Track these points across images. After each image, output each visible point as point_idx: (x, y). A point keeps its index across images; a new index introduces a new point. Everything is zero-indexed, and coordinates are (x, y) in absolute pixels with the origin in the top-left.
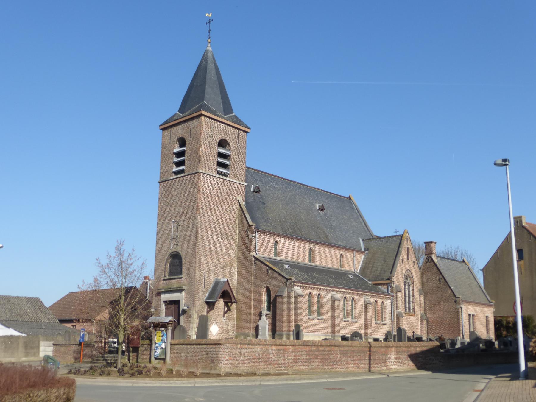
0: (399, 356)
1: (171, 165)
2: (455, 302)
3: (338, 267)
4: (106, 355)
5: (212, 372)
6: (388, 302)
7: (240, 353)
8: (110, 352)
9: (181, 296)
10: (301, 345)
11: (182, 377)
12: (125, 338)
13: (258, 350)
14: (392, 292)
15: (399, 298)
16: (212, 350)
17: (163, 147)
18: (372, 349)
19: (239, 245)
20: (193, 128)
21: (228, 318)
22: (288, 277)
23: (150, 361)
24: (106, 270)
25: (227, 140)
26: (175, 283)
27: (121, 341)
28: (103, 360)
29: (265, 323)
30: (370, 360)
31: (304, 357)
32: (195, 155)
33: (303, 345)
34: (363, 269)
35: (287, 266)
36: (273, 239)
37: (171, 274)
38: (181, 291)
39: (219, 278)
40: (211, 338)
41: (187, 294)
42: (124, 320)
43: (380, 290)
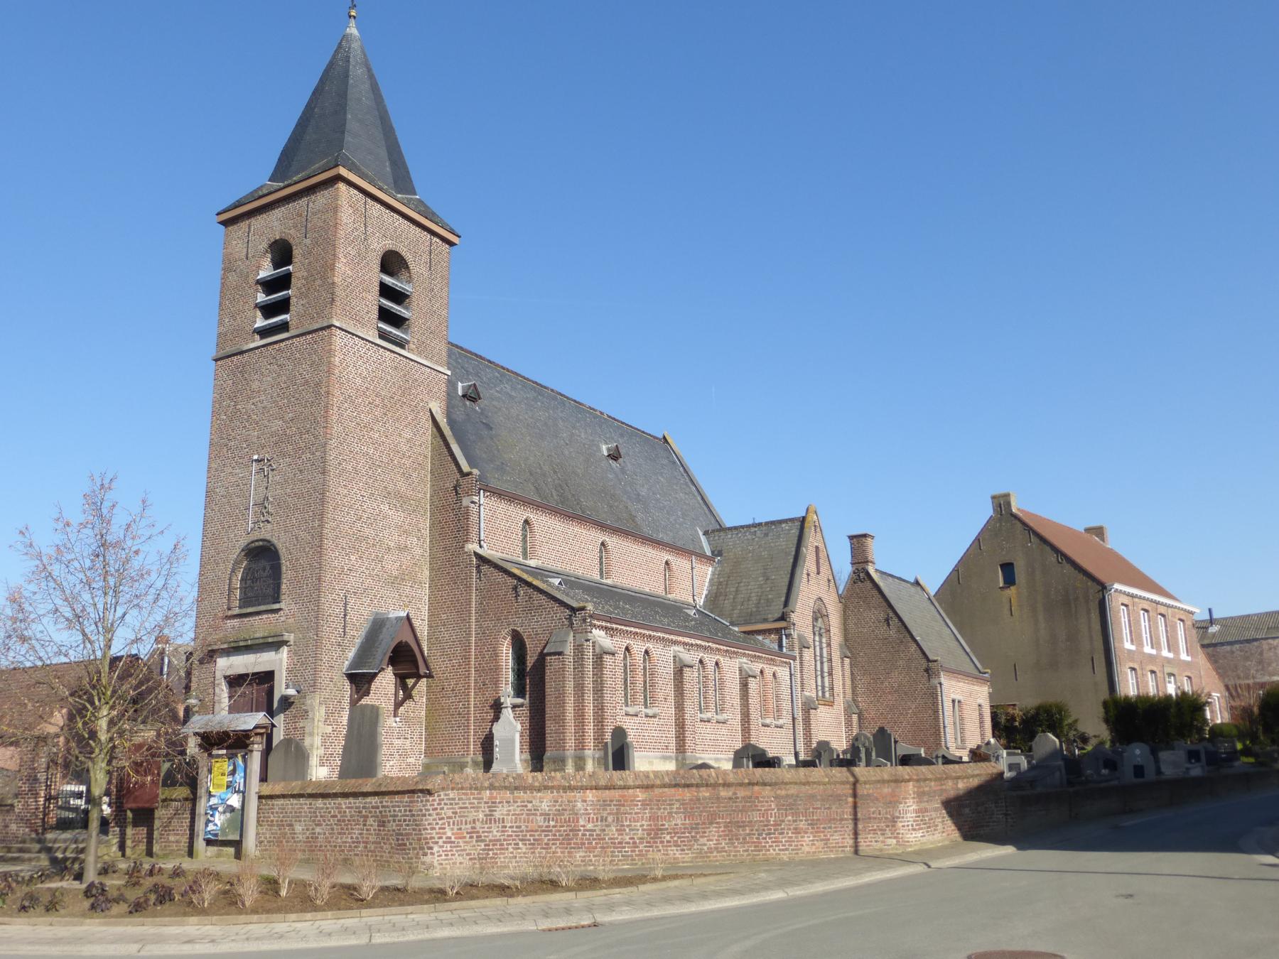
0: (924, 805)
1: (250, 314)
2: (927, 670)
3: (660, 591)
4: (49, 836)
5: (416, 883)
6: (783, 673)
7: (490, 818)
8: (64, 825)
9: (277, 661)
10: (670, 786)
11: (316, 909)
12: (109, 782)
13: (545, 806)
14: (791, 648)
15: (805, 664)
16: (400, 812)
17: (228, 268)
18: (862, 790)
19: (432, 526)
20: (314, 214)
21: (406, 720)
22: (575, 605)
23: (191, 853)
24: (56, 569)
25: (403, 254)
26: (260, 626)
27: (97, 791)
28: (39, 852)
29: (511, 730)
30: (856, 820)
31: (679, 820)
32: (318, 282)
33: (676, 785)
34: (714, 599)
35: (556, 581)
36: (519, 514)
37: (245, 602)
38: (276, 645)
39: (383, 610)
40: (392, 774)
41: (294, 653)
42: (112, 723)
43: (763, 645)
